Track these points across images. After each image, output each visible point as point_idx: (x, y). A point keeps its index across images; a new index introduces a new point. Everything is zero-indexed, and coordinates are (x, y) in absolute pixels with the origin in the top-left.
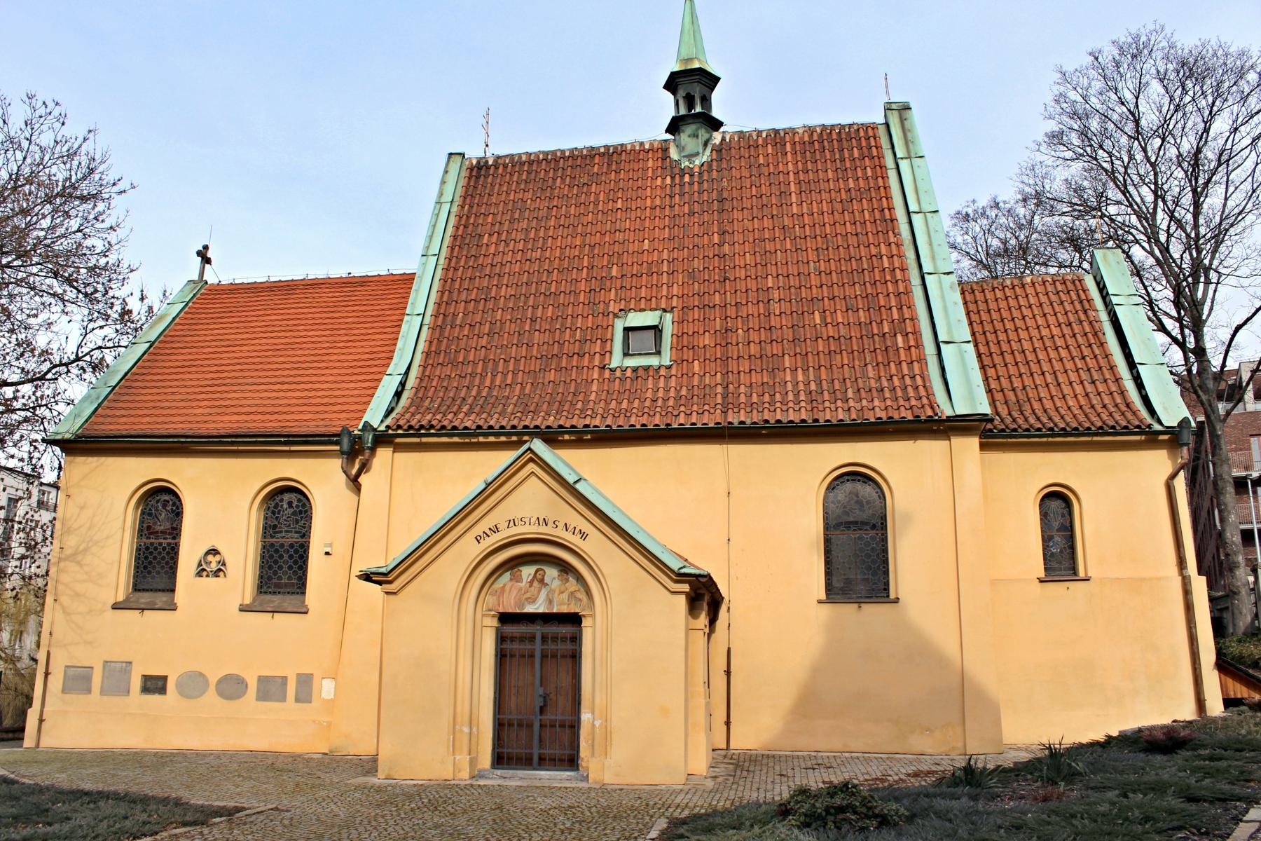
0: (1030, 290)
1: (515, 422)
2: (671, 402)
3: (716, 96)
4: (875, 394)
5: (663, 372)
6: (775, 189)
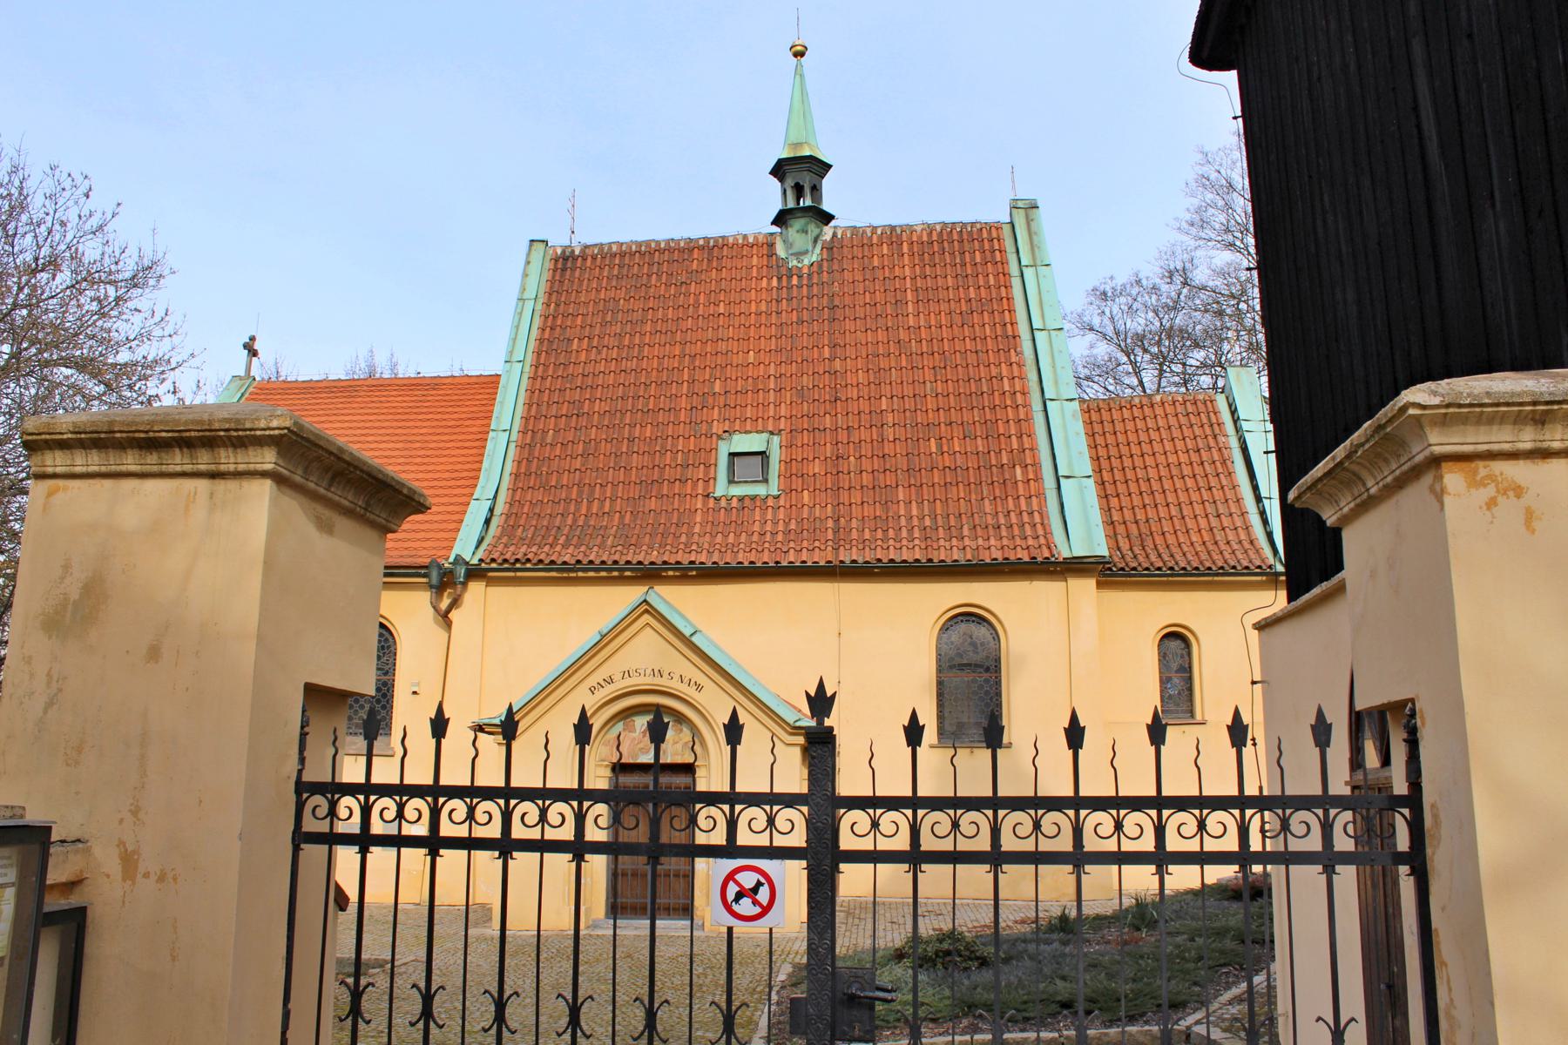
0: (1159, 411)
1: (616, 557)
2: (780, 537)
3: (827, 183)
4: (991, 532)
5: (770, 502)
6: (890, 297)
